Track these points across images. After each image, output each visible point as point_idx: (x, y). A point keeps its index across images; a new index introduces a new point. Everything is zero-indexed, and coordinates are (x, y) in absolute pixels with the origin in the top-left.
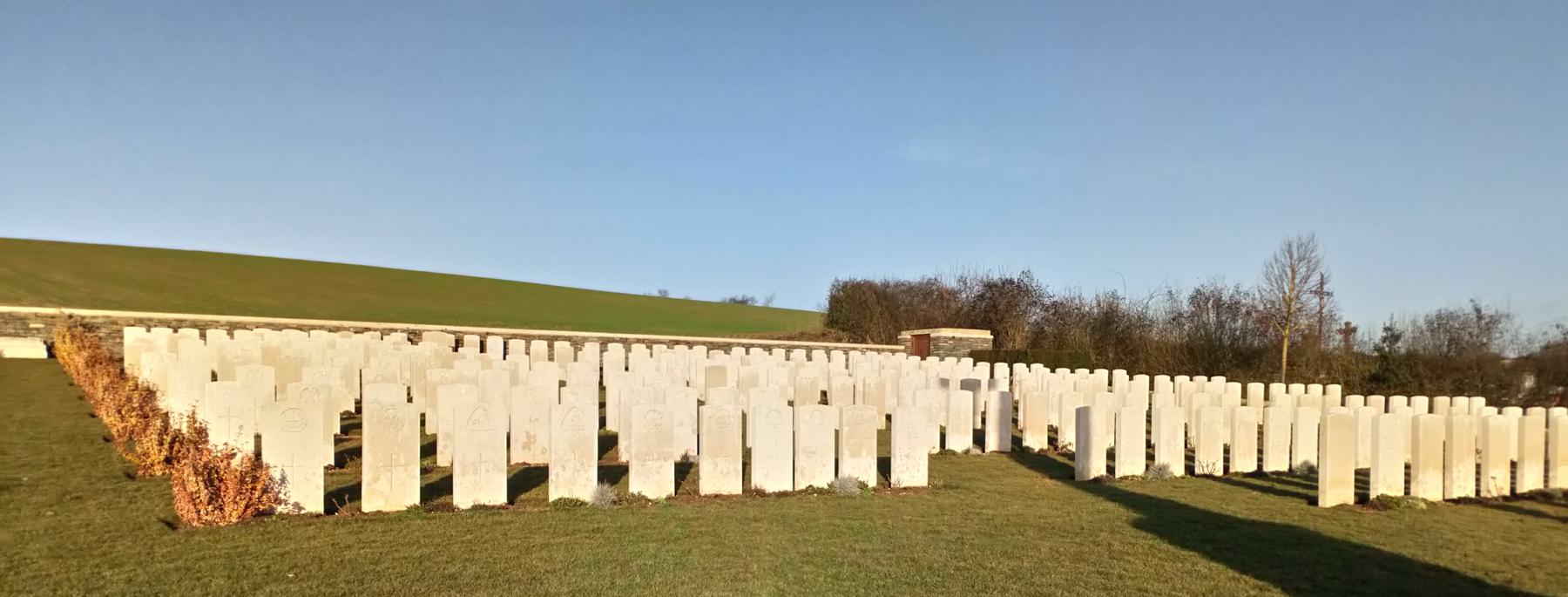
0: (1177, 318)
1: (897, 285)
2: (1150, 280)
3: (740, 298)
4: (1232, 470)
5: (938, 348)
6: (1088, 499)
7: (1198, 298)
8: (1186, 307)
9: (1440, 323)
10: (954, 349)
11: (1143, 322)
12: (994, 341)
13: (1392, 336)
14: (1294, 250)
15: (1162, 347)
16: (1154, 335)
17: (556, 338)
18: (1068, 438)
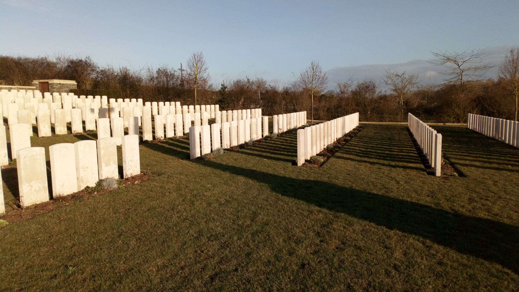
0: (152, 79)
1: (26, 59)
2: (142, 64)
5: (54, 88)
6: (194, 165)
7: (159, 71)
8: (155, 75)
9: (238, 83)
10: (60, 89)
11: (139, 80)
12: (78, 85)
13: (224, 88)
14: (196, 57)
15: (147, 88)
16: (143, 84)
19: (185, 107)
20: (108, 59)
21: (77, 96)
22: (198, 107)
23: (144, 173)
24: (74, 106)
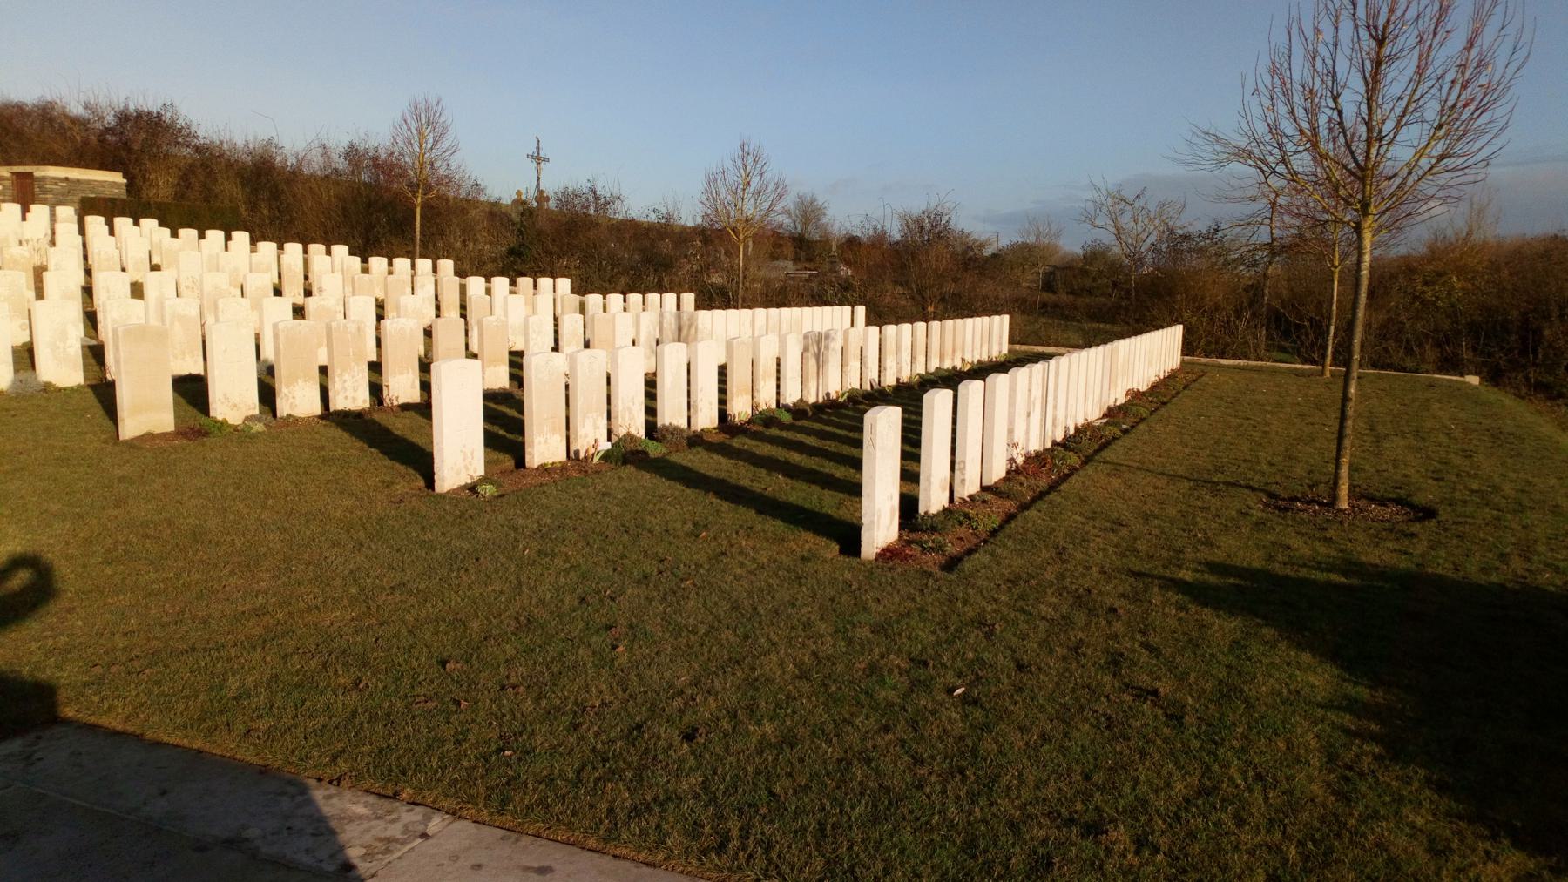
4: (332, 408)
5: (45, 192)
18: (402, 387)
19: (594, 300)
20: (228, 110)
21: (167, 231)
22: (424, 264)
24: (155, 261)
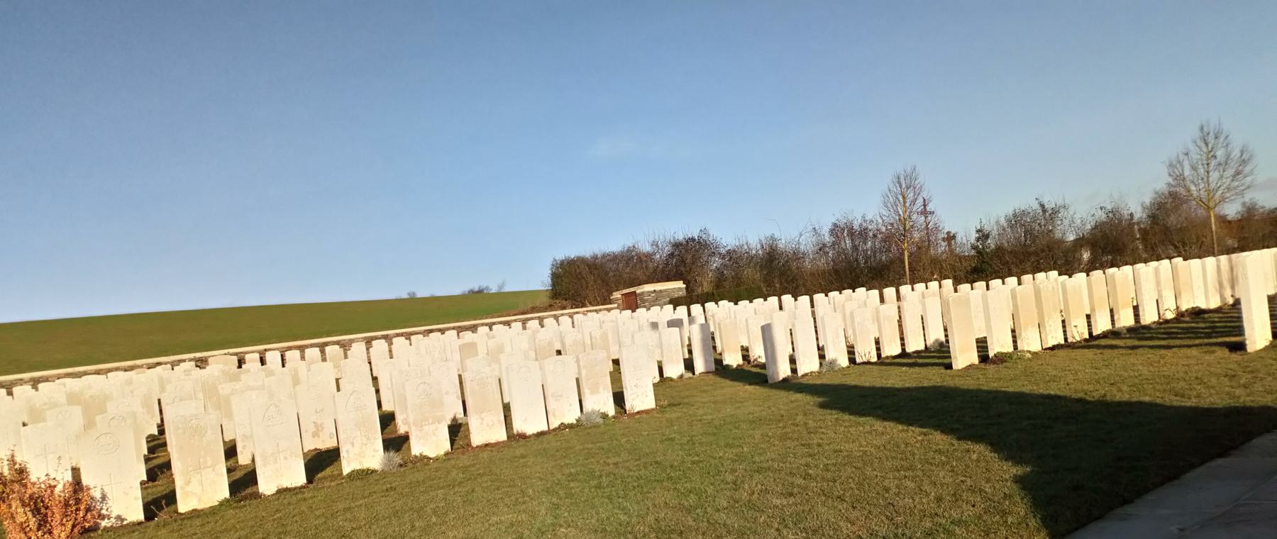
0: (822, 248)
1: (604, 256)
2: (799, 225)
3: (476, 289)
6: (782, 395)
8: (828, 239)
10: (657, 299)
11: (797, 256)
12: (687, 288)
17: (326, 344)
20: (737, 229)
23: (660, 408)
